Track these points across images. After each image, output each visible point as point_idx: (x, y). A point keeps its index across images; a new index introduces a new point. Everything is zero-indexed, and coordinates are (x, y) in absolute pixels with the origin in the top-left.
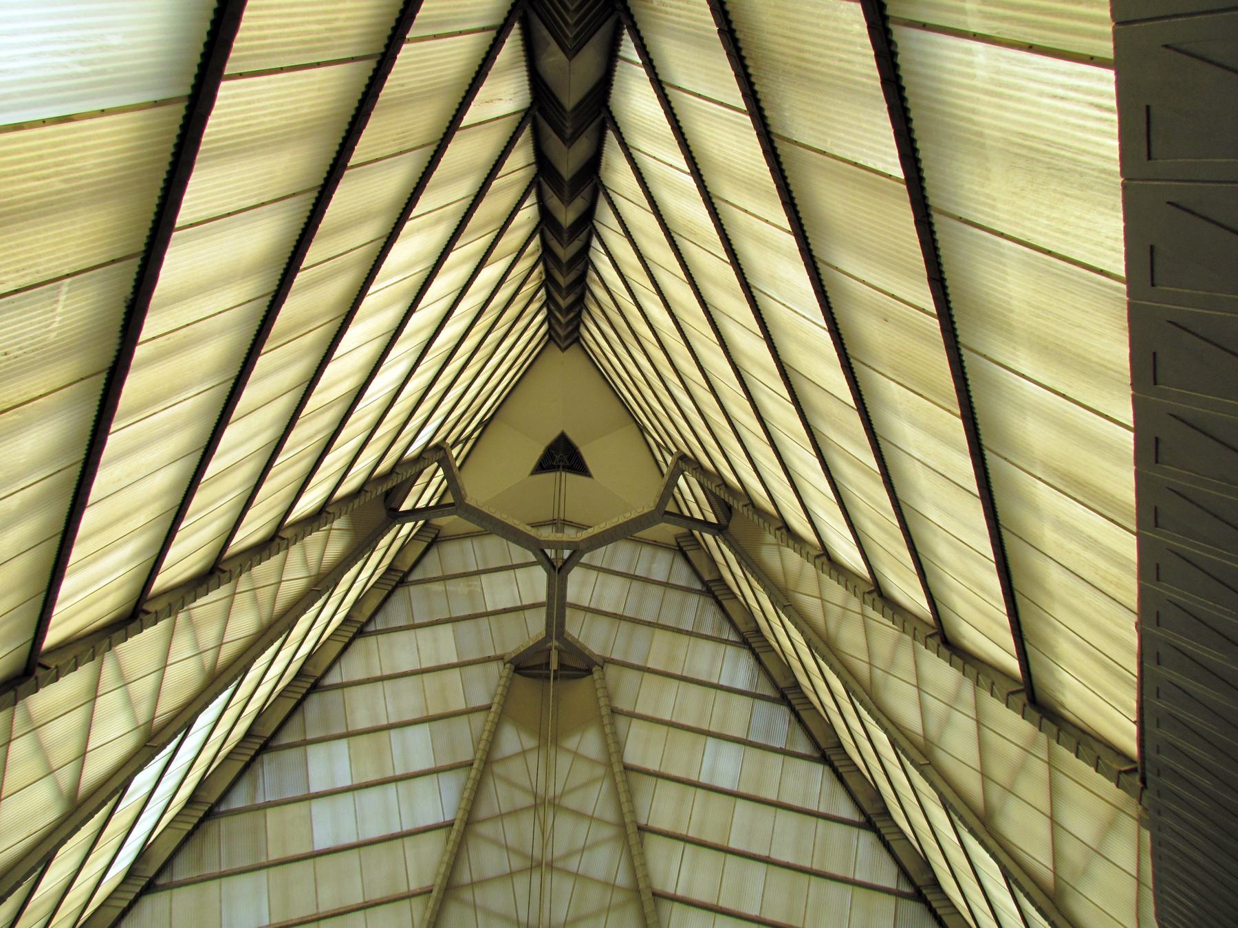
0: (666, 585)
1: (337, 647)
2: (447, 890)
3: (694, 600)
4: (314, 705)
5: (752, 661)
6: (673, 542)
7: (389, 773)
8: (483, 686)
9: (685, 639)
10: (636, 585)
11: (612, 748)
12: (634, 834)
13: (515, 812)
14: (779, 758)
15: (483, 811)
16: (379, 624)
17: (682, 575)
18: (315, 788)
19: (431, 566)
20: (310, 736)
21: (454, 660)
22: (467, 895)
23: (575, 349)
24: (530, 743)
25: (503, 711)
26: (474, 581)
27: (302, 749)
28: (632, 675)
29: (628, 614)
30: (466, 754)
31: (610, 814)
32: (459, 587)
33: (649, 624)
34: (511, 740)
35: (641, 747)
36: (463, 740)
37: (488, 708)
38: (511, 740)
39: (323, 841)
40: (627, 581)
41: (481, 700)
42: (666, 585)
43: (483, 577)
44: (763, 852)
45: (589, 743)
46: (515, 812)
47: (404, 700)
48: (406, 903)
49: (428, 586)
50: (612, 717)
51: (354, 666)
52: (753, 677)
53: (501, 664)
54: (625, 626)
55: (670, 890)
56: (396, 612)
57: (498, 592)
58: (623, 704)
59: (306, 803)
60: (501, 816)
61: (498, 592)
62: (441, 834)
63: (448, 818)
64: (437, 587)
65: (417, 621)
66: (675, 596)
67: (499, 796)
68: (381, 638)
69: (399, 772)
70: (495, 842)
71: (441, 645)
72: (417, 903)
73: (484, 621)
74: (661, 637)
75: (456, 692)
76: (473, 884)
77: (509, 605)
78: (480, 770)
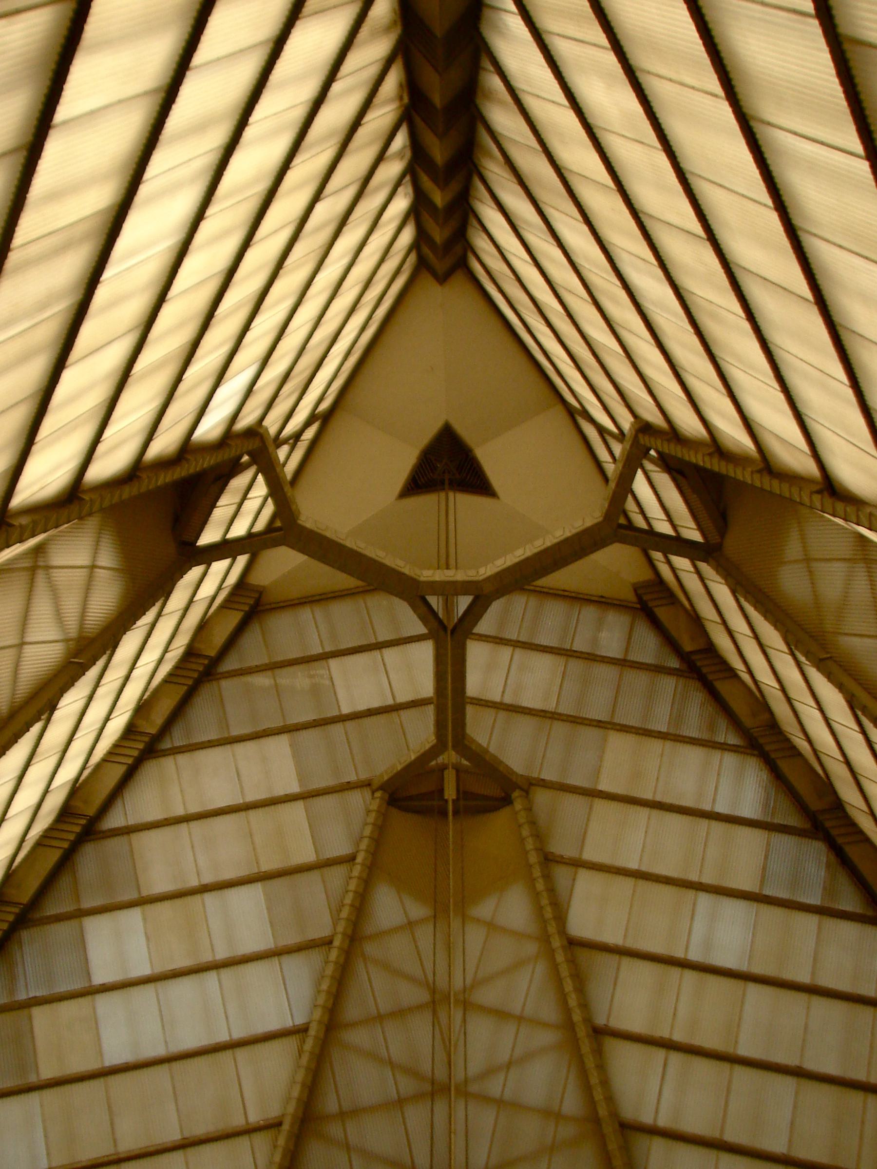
0: (623, 663)
1: (116, 772)
2: (305, 1122)
3: (668, 685)
4: (89, 859)
5: (765, 775)
6: (631, 597)
7: (206, 957)
8: (343, 826)
9: (656, 745)
10: (575, 666)
11: (549, 913)
12: (589, 1039)
13: (400, 1013)
14: (812, 920)
15: (352, 1011)
16: (177, 738)
17: (647, 647)
18: (100, 977)
19: (253, 649)
20: (86, 904)
21: (294, 788)
22: (335, 1130)
23: (458, 281)
24: (418, 910)
25: (374, 864)
26: (319, 669)
27: (74, 923)
28: (572, 804)
29: (563, 709)
30: (321, 925)
31: (549, 1012)
32: (297, 680)
33: (599, 724)
34: (389, 907)
35: (596, 909)
36: (318, 907)
37: (351, 859)
38: (389, 907)
39: (116, 1052)
40: (561, 660)
41: (339, 847)
42: (623, 663)
43: (333, 663)
44: (804, 978)
45: (514, 908)
46: (400, 1013)
47: (223, 849)
48: (243, 1143)
49: (249, 679)
50: (548, 869)
51: (144, 802)
52: (767, 799)
53: (367, 793)
54: (560, 729)
55: (647, 1118)
56: (203, 720)
57: (358, 684)
58: (562, 846)
59: (89, 998)
60: (380, 1018)
61: (358, 684)
62: (289, 1045)
63: (300, 1020)
64: (262, 680)
65: (235, 732)
66: (639, 680)
67: (374, 988)
68: (182, 759)
69: (221, 954)
70: (373, 1056)
71: (272, 767)
72: (261, 1141)
73: (337, 730)
74: (617, 742)
75: (296, 836)
76: (343, 1115)
77: (376, 704)
78: (346, 951)
